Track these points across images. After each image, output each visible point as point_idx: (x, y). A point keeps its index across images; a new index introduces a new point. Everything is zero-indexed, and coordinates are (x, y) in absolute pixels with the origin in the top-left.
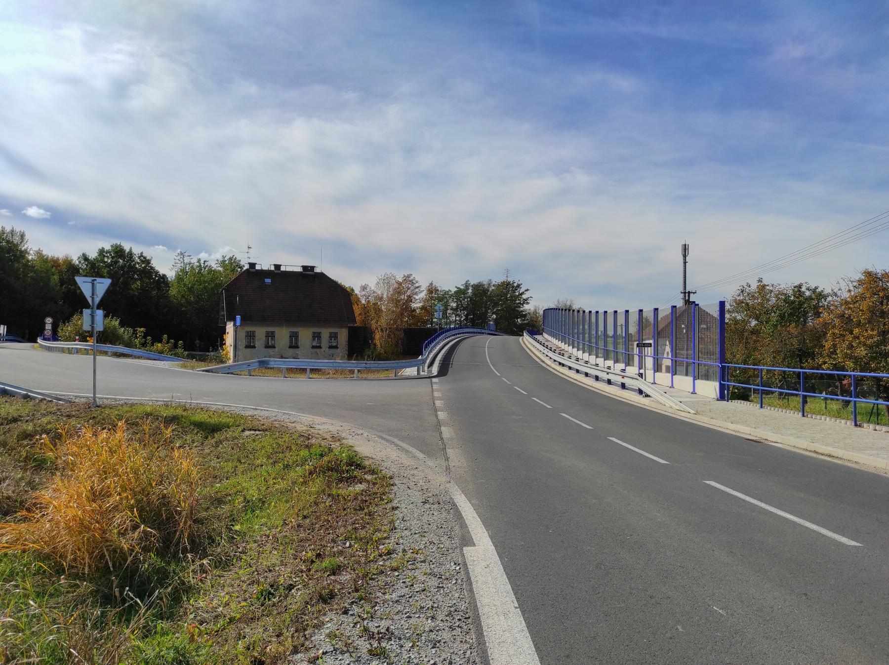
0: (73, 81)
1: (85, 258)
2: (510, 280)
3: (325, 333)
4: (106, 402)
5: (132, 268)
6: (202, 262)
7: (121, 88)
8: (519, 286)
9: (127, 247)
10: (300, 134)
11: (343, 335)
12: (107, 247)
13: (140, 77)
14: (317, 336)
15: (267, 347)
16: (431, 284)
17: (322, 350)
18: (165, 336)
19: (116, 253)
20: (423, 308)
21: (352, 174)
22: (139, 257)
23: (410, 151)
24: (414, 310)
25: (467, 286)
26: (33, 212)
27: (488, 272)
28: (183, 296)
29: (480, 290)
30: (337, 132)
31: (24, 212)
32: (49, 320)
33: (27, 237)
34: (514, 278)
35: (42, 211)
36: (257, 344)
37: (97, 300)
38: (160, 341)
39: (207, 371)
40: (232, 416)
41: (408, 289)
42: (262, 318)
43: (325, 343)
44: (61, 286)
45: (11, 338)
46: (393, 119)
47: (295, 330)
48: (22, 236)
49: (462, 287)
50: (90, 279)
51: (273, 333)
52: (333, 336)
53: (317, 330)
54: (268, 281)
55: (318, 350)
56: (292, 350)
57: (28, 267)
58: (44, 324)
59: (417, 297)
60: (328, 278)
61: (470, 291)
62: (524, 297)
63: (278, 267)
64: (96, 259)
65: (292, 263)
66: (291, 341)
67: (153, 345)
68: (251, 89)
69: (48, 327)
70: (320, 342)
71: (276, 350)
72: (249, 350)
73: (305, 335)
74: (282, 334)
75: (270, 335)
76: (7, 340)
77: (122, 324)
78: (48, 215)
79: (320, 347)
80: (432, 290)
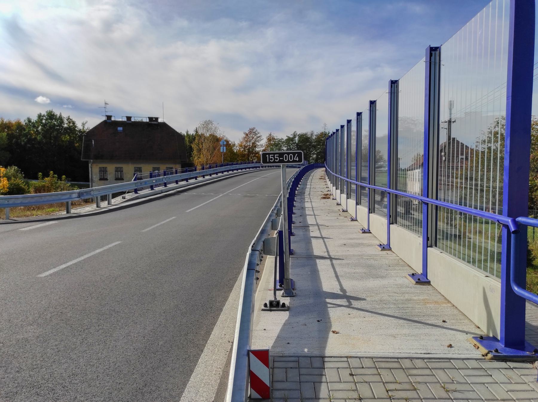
0: (81, 23)
2: (327, 131)
7: (108, 26)
9: (57, 112)
10: (213, 49)
12: (44, 113)
13: (119, 19)
16: (270, 135)
18: (52, 172)
21: (245, 73)
23: (280, 57)
24: (258, 153)
25: (295, 136)
30: (236, 47)
36: (109, 177)
38: (48, 176)
41: (253, 138)
42: (112, 158)
46: (270, 37)
49: (291, 136)
53: (156, 166)
54: (120, 129)
60: (170, 127)
61: (297, 139)
63: (129, 118)
65: (141, 114)
67: (43, 179)
68: (183, 23)
78: (48, 101)
80: (270, 139)
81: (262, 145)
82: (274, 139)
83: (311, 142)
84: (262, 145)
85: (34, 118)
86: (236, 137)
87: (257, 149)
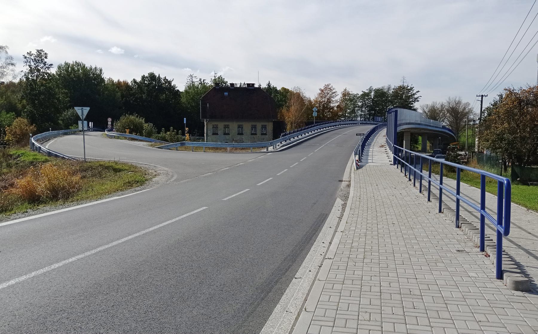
1: (135, 81)
2: (406, 85)
3: (259, 125)
4: (92, 160)
5: (160, 86)
6: (202, 80)
8: (411, 89)
11: (270, 127)
12: (146, 75)
14: (254, 127)
15: (225, 134)
16: (346, 90)
17: (258, 136)
19: (151, 78)
20: (338, 107)
22: (164, 80)
24: (333, 108)
26: (114, 50)
27: (388, 82)
28: (189, 103)
29: (380, 94)
31: (110, 50)
32: (110, 120)
33: (103, 71)
34: (409, 84)
35: (119, 49)
37: (84, 117)
38: (169, 131)
39: (159, 148)
40: (124, 164)
42: (222, 117)
43: (259, 132)
44: (122, 99)
45: (96, 129)
47: (241, 124)
48: (101, 70)
49: (367, 91)
50: (80, 108)
51: (228, 125)
52: (264, 127)
53: (254, 124)
54: (226, 94)
55: (255, 136)
56: (239, 136)
57: (106, 87)
58: (108, 122)
59: (334, 100)
62: (416, 96)
64: (140, 82)
66: (239, 131)
69: (110, 123)
70: (256, 131)
71: (230, 136)
72: (215, 136)
73: (247, 127)
74: (234, 126)
75: (226, 127)
76: (94, 131)
77: (146, 122)
78: (123, 52)
79: (256, 134)
80: (345, 94)
81: (336, 100)
82: (349, 94)
83: (388, 97)
84: (337, 101)
85: (139, 79)
86: (311, 93)
87: (332, 105)
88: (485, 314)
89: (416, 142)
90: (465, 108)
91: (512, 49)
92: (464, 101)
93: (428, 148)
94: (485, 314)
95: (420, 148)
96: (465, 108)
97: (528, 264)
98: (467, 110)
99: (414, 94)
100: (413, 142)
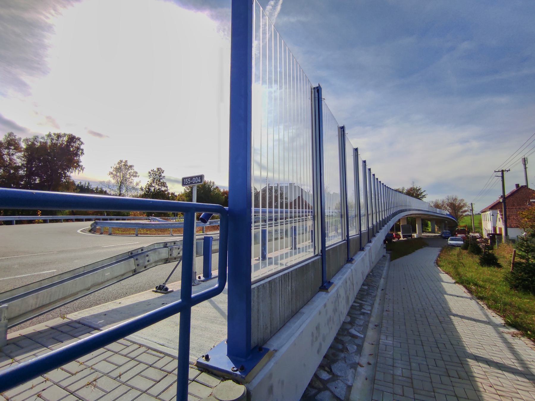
2: (415, 187)
8: (419, 189)
62: (423, 194)
88: (105, 360)
89: (427, 225)
90: (460, 204)
91: (504, 164)
92: (459, 198)
93: (436, 230)
94: (105, 360)
95: (430, 230)
96: (460, 204)
97: (218, 315)
98: (462, 204)
99: (422, 193)
100: (424, 225)
